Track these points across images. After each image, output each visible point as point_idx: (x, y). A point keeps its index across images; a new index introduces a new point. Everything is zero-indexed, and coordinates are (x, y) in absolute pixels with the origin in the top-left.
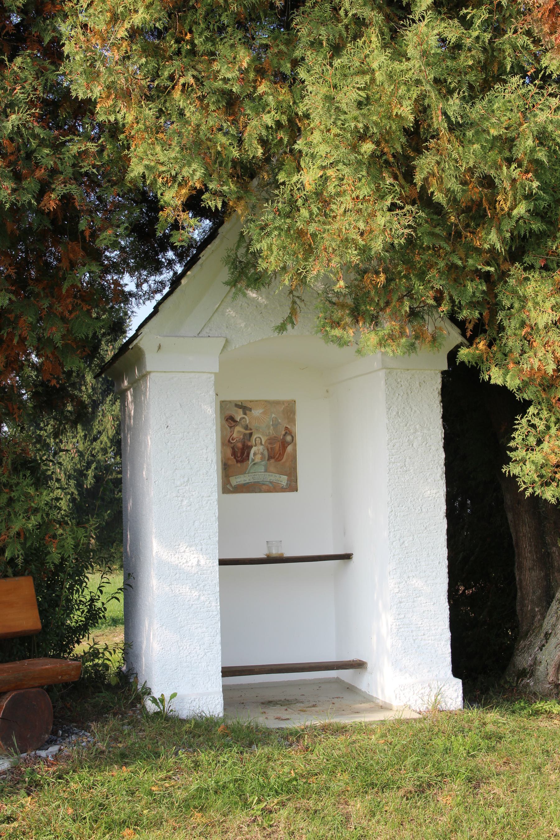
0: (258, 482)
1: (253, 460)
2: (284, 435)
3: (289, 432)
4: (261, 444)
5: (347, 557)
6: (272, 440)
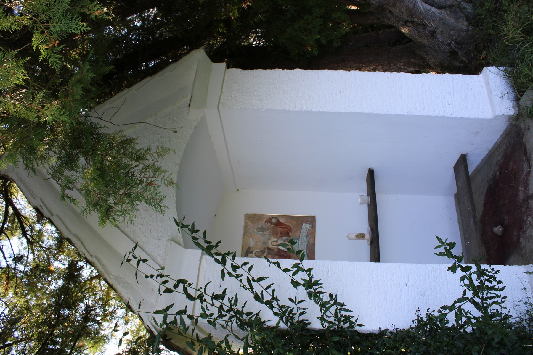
0: (307, 246)
2: (271, 223)
3: (269, 220)
4: (277, 241)
5: (371, 173)
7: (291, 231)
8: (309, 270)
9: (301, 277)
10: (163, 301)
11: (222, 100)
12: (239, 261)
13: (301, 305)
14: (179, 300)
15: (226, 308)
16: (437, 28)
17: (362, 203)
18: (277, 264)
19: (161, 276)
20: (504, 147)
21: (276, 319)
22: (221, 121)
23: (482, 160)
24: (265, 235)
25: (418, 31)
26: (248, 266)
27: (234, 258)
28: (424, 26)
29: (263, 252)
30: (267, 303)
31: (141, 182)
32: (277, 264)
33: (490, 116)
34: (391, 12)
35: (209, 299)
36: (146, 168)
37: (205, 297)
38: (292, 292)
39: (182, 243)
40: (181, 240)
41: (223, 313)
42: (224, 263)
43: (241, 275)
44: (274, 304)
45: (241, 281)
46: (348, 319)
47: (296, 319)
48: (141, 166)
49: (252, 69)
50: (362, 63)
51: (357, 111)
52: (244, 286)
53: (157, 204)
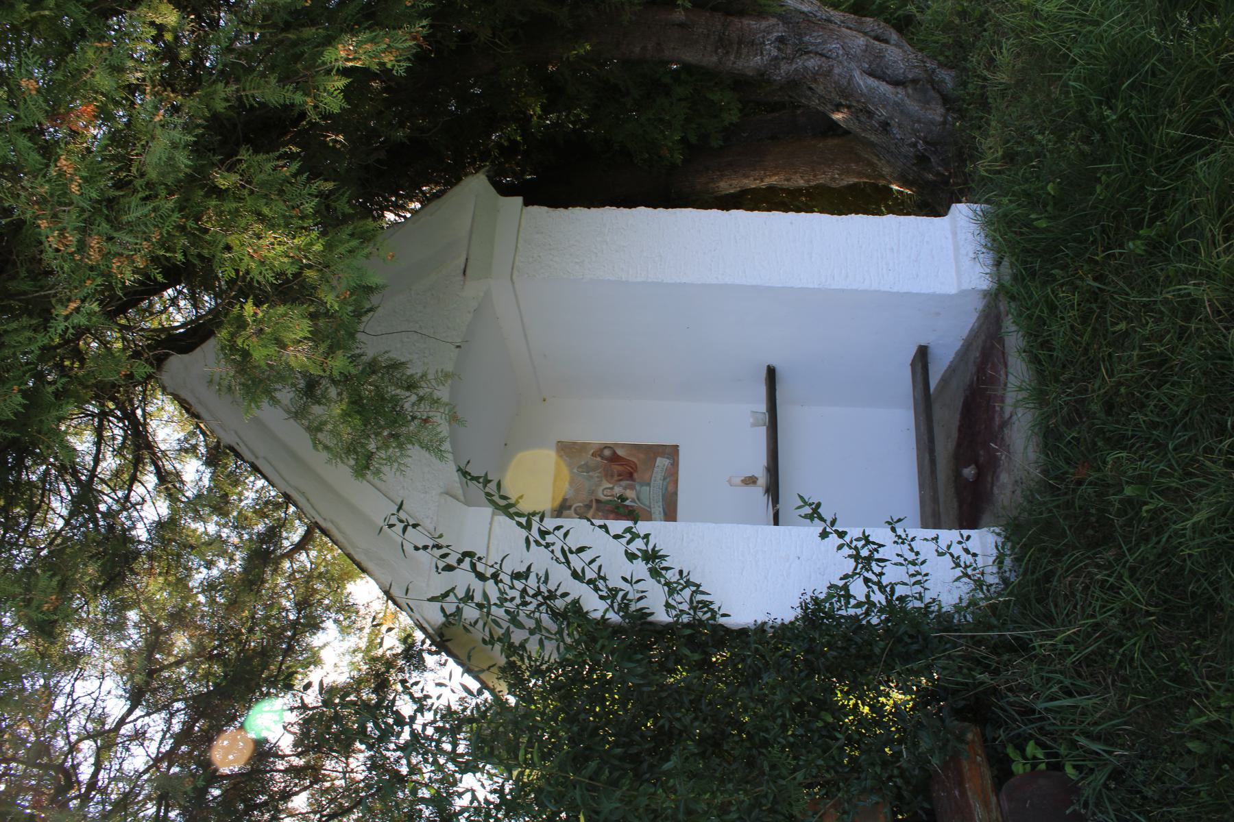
0: (663, 496)
1: (633, 501)
2: (602, 458)
3: (599, 451)
4: (612, 489)
5: (771, 373)
6: (608, 475)
7: (636, 471)
8: (647, 536)
9: (639, 544)
10: (440, 583)
11: (517, 263)
12: (549, 524)
13: (640, 586)
14: (463, 579)
15: (531, 592)
16: (892, 118)
17: (754, 425)
18: (605, 528)
19: (438, 547)
20: (983, 337)
21: (602, 606)
22: (516, 296)
23: (957, 354)
24: (591, 477)
25: (860, 122)
26: (563, 531)
27: (542, 520)
28: (870, 114)
29: (589, 507)
30: (590, 582)
31: (414, 418)
32: (604, 527)
33: (953, 290)
34: (810, 89)
35: (506, 579)
36: (421, 399)
37: (502, 576)
38: (627, 568)
39: (462, 498)
40: (459, 492)
41: (528, 599)
42: (528, 527)
43: (553, 544)
44: (601, 584)
45: (552, 552)
46: (706, 604)
47: (633, 607)
48: (414, 398)
49: (566, 207)
50: (765, 170)
51: (737, 282)
52: (557, 560)
53: (433, 448)
